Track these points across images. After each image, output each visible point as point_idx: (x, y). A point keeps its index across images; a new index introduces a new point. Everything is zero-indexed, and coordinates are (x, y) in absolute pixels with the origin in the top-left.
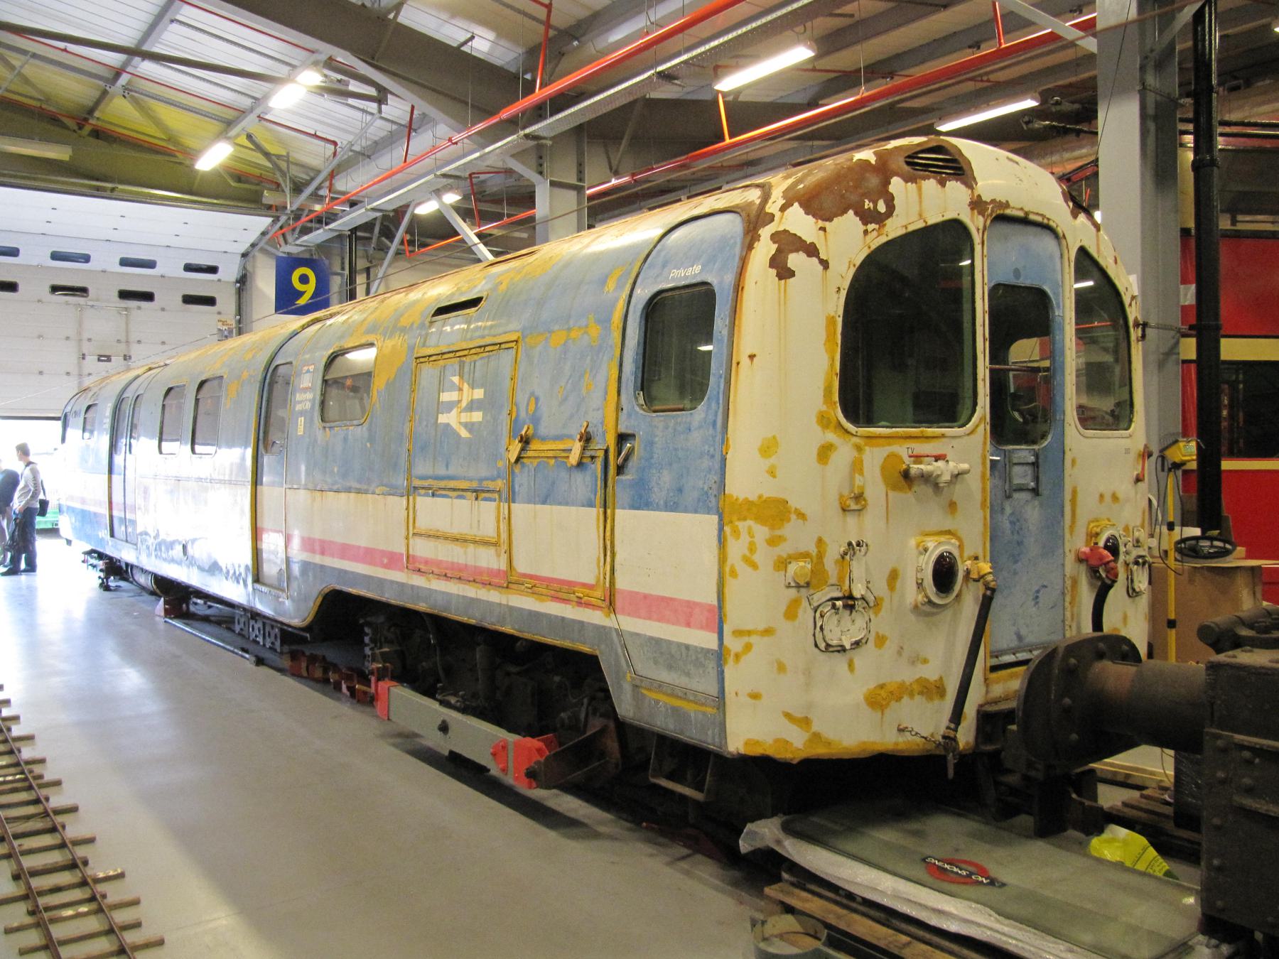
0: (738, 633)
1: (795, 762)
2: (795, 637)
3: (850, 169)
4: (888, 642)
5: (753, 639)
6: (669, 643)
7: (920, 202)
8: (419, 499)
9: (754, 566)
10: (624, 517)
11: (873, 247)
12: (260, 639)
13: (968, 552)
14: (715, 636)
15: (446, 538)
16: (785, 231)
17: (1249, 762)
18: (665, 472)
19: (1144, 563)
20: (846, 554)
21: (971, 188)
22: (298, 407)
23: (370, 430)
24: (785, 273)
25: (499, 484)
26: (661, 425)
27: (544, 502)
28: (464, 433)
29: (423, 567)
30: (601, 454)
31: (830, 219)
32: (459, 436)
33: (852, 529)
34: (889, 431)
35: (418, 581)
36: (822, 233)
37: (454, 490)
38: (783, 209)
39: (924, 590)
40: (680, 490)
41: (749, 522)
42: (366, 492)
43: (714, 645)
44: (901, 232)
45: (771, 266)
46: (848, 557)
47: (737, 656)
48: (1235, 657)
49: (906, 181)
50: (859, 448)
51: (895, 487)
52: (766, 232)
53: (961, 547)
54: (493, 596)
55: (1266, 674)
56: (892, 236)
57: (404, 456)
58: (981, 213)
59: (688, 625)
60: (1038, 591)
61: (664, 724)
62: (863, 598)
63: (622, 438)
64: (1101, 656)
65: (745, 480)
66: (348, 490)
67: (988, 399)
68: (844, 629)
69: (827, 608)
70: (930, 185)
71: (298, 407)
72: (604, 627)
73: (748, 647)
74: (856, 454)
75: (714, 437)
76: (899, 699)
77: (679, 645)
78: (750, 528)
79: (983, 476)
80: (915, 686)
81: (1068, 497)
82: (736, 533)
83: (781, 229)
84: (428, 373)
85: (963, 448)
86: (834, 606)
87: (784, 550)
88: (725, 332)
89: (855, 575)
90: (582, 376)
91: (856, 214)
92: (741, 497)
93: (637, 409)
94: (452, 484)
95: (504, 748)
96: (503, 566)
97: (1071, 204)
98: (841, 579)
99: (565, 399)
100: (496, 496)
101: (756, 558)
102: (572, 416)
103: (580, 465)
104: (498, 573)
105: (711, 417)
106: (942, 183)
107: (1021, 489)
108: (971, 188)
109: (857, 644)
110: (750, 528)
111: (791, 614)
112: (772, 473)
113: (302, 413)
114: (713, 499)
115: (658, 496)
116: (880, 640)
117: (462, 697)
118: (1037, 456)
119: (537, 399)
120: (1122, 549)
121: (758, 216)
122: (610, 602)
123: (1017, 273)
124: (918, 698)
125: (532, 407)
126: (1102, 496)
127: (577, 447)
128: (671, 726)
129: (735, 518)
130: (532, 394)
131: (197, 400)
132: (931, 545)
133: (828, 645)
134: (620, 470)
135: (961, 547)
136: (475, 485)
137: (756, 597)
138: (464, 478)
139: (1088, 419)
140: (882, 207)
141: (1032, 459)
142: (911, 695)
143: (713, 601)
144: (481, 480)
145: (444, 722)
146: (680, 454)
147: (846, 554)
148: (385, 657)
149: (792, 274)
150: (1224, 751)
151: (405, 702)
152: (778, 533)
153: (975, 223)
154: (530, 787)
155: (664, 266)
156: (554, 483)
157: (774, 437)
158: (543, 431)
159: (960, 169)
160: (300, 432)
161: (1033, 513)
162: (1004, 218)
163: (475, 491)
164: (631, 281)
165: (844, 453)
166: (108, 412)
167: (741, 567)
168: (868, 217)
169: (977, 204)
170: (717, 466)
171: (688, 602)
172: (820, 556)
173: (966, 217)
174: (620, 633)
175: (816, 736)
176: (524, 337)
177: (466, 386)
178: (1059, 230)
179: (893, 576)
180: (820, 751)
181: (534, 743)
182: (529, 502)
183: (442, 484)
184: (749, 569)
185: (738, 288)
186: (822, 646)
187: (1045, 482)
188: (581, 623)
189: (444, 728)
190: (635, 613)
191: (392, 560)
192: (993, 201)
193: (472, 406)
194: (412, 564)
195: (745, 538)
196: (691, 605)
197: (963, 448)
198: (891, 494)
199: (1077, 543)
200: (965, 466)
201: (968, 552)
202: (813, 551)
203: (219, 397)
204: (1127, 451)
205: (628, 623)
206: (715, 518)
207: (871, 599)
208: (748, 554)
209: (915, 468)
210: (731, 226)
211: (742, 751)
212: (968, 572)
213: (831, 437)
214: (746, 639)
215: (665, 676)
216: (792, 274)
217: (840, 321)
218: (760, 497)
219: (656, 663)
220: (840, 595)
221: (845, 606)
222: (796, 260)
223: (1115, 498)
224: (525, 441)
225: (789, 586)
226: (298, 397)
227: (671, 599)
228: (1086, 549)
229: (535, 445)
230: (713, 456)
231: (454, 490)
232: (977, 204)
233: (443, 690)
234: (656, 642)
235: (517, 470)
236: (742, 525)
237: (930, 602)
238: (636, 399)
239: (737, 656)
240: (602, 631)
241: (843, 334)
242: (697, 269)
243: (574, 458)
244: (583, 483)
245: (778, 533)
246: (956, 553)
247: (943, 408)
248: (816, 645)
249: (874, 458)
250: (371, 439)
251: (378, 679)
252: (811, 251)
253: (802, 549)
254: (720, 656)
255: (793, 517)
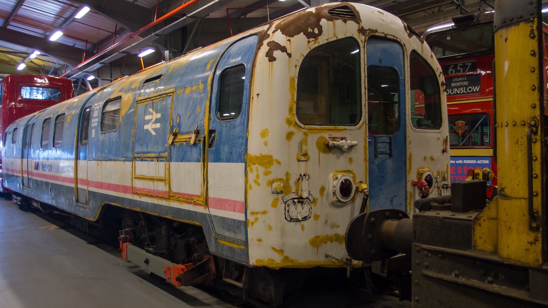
0: (253, 213)
1: (277, 269)
2: (276, 215)
3: (304, 15)
4: (320, 218)
5: (259, 216)
6: (228, 219)
7: (335, 29)
8: (137, 162)
9: (259, 184)
10: (211, 166)
11: (312, 48)
12: (80, 228)
13: (358, 180)
14: (244, 215)
15: (146, 179)
16: (273, 41)
17: (427, 256)
18: (226, 146)
19: (447, 188)
20: (299, 179)
21: (359, 24)
22: (93, 125)
23: (119, 134)
24: (272, 59)
25: (166, 154)
26: (225, 125)
27: (182, 161)
28: (153, 133)
29: (138, 192)
30: (202, 139)
31: (292, 36)
32: (151, 134)
33: (302, 168)
34: (320, 127)
35: (136, 198)
36: (288, 42)
37: (150, 158)
38: (273, 32)
39: (336, 195)
40: (231, 153)
41: (257, 165)
42: (117, 160)
43: (244, 219)
44: (326, 42)
45: (266, 56)
46: (300, 181)
47: (252, 223)
48: (439, 214)
49: (328, 20)
50: (306, 134)
51: (324, 152)
52: (265, 42)
53: (354, 177)
54: (164, 203)
55: (433, 219)
56: (321, 44)
57: (131, 144)
58: (364, 34)
59: (234, 211)
60: (392, 198)
61: (226, 254)
62: (307, 198)
63: (211, 132)
64: (388, 218)
65: (255, 147)
66: (110, 160)
67: (367, 114)
68: (298, 211)
69: (290, 202)
70: (339, 22)
71: (93, 125)
72: (204, 214)
73: (256, 219)
74: (304, 136)
75: (244, 129)
76: (326, 243)
77: (231, 220)
78: (257, 168)
79: (365, 147)
80: (333, 237)
81: (408, 157)
82: (251, 170)
83: (272, 40)
84: (141, 106)
85: (356, 136)
86: (294, 202)
87: (271, 177)
88: (248, 85)
89: (303, 188)
90: (197, 106)
91: (304, 34)
92: (253, 155)
93: (216, 119)
94: (150, 155)
95: (169, 269)
96: (167, 190)
97: (408, 32)
98: (297, 190)
99: (190, 116)
100: (165, 159)
101: (260, 181)
102: (192, 124)
103: (195, 144)
104: (163, 192)
105: (242, 121)
106: (345, 21)
107: (382, 153)
108: (359, 24)
109: (305, 218)
110: (257, 168)
111: (274, 205)
112: (266, 144)
113: (94, 127)
114: (243, 156)
115: (223, 156)
116: (317, 217)
117: (154, 248)
118: (390, 139)
119: (180, 117)
120: (434, 181)
121: (264, 35)
122: (206, 203)
123: (380, 61)
124: (334, 242)
125: (178, 120)
126: (425, 158)
127: (193, 136)
128: (229, 255)
129: (251, 164)
130: (178, 115)
131: (55, 124)
132: (339, 176)
133: (291, 219)
134: (210, 146)
135: (354, 177)
136: (157, 155)
137: (260, 198)
138: (153, 152)
139: (419, 124)
140: (316, 31)
141: (389, 141)
142: (332, 241)
143: (243, 200)
144: (159, 153)
145: (147, 259)
146: (232, 138)
147: (299, 179)
148: (126, 233)
149: (275, 59)
150: (419, 251)
151: (135, 253)
152: (268, 170)
153: (361, 39)
154: (179, 285)
155: (228, 58)
156: (185, 152)
157: (267, 129)
158: (182, 130)
159: (354, 15)
160: (93, 136)
161: (390, 163)
162: (374, 37)
163: (157, 158)
164: (215, 65)
165: (298, 136)
166: (22, 131)
167: (253, 185)
168: (309, 35)
169: (362, 31)
170: (245, 142)
171: (234, 201)
172: (288, 180)
173: (356, 35)
174: (210, 216)
175: (286, 258)
176: (176, 90)
177: (154, 113)
178: (402, 43)
179: (323, 189)
180: (288, 264)
181: (181, 266)
182: (176, 161)
183: (146, 155)
184: (257, 185)
185: (253, 66)
186: (289, 219)
187: (398, 152)
188: (196, 212)
189: (147, 262)
190: (215, 207)
191: (125, 189)
192: (369, 29)
193: (157, 121)
194: (135, 191)
195: (255, 172)
196: (235, 202)
197: (356, 136)
198: (322, 155)
199: (412, 177)
200: (355, 142)
201: (358, 180)
202: (284, 178)
203: (63, 122)
204: (438, 139)
205: (214, 212)
206: (244, 164)
207: (311, 198)
208: (256, 179)
209: (331, 143)
210: (254, 40)
211: (255, 264)
212: (357, 188)
213: (292, 129)
214: (256, 216)
215: (227, 234)
216: (275, 59)
217: (296, 80)
218: (261, 154)
219: (223, 228)
220: (297, 197)
221: (299, 202)
222: (277, 54)
223: (432, 159)
224: (175, 135)
225: (273, 193)
226: (93, 121)
227: (228, 200)
228: (416, 180)
229: (179, 137)
230: (243, 138)
231: (150, 158)
232: (362, 31)
233: (148, 245)
234: (223, 219)
235: (172, 148)
236: (254, 167)
237: (339, 201)
238: (216, 115)
239: (252, 223)
240: (203, 215)
241: (298, 85)
242: (240, 58)
243: (192, 142)
244: (195, 152)
245: (268, 170)
246: (351, 180)
247: (353, 120)
248: (286, 218)
249: (313, 139)
250: (119, 137)
251: (123, 242)
252: (284, 49)
253: (279, 177)
254: (245, 224)
255: (275, 163)
